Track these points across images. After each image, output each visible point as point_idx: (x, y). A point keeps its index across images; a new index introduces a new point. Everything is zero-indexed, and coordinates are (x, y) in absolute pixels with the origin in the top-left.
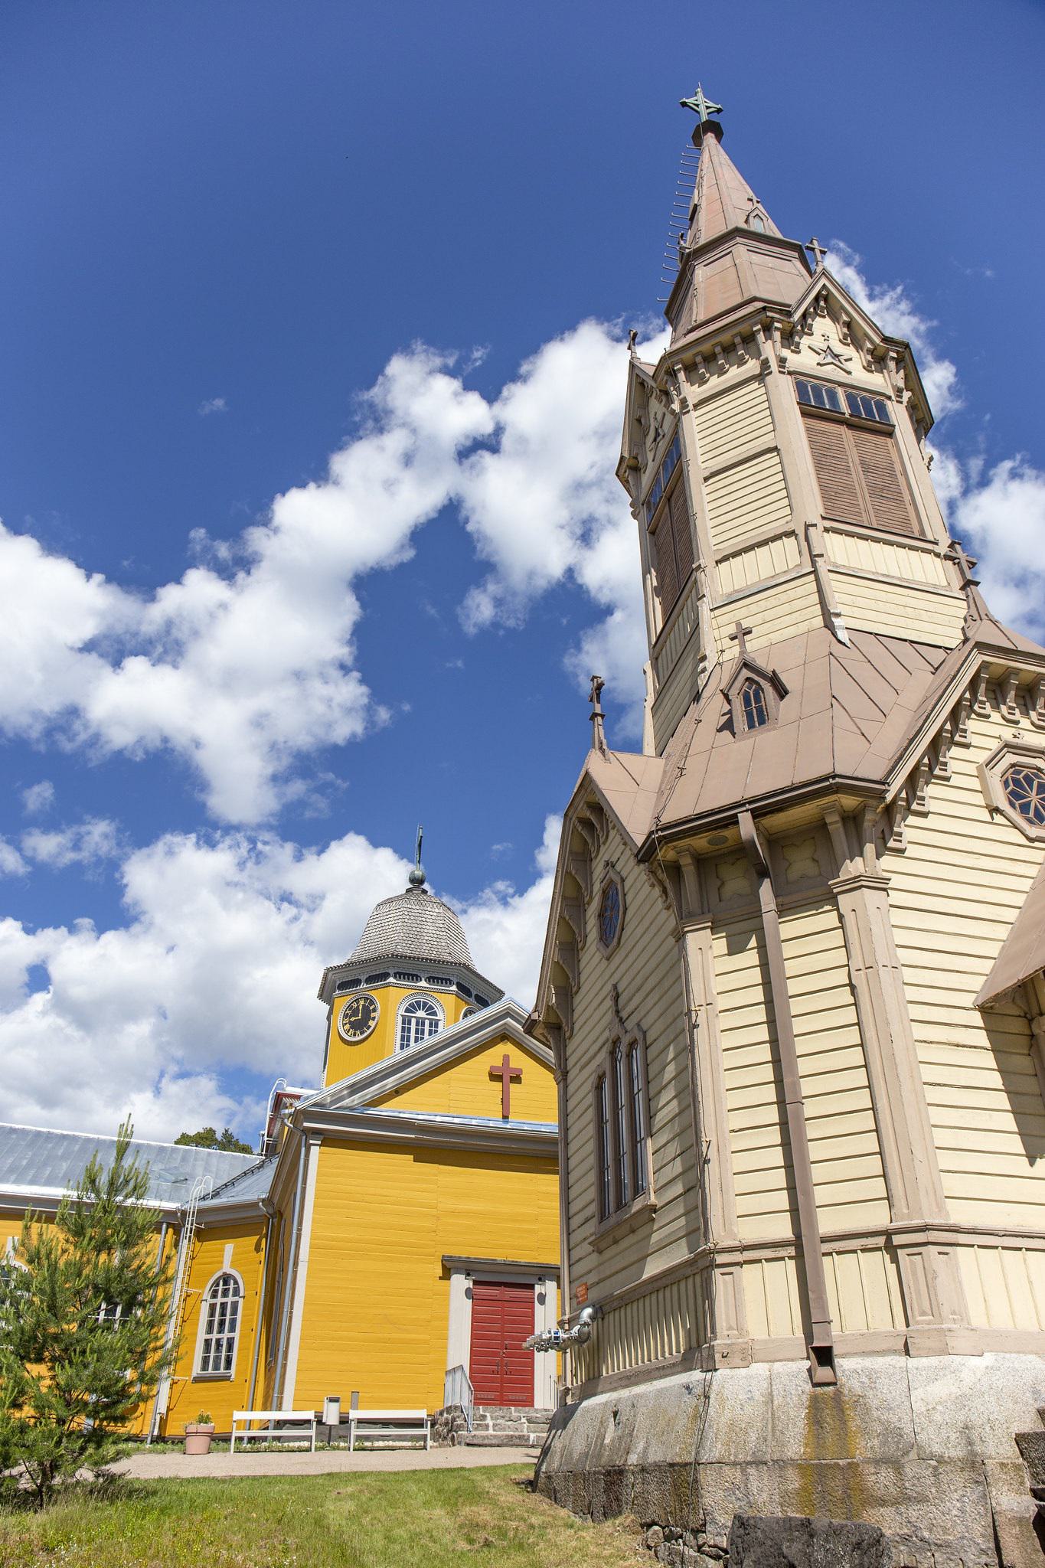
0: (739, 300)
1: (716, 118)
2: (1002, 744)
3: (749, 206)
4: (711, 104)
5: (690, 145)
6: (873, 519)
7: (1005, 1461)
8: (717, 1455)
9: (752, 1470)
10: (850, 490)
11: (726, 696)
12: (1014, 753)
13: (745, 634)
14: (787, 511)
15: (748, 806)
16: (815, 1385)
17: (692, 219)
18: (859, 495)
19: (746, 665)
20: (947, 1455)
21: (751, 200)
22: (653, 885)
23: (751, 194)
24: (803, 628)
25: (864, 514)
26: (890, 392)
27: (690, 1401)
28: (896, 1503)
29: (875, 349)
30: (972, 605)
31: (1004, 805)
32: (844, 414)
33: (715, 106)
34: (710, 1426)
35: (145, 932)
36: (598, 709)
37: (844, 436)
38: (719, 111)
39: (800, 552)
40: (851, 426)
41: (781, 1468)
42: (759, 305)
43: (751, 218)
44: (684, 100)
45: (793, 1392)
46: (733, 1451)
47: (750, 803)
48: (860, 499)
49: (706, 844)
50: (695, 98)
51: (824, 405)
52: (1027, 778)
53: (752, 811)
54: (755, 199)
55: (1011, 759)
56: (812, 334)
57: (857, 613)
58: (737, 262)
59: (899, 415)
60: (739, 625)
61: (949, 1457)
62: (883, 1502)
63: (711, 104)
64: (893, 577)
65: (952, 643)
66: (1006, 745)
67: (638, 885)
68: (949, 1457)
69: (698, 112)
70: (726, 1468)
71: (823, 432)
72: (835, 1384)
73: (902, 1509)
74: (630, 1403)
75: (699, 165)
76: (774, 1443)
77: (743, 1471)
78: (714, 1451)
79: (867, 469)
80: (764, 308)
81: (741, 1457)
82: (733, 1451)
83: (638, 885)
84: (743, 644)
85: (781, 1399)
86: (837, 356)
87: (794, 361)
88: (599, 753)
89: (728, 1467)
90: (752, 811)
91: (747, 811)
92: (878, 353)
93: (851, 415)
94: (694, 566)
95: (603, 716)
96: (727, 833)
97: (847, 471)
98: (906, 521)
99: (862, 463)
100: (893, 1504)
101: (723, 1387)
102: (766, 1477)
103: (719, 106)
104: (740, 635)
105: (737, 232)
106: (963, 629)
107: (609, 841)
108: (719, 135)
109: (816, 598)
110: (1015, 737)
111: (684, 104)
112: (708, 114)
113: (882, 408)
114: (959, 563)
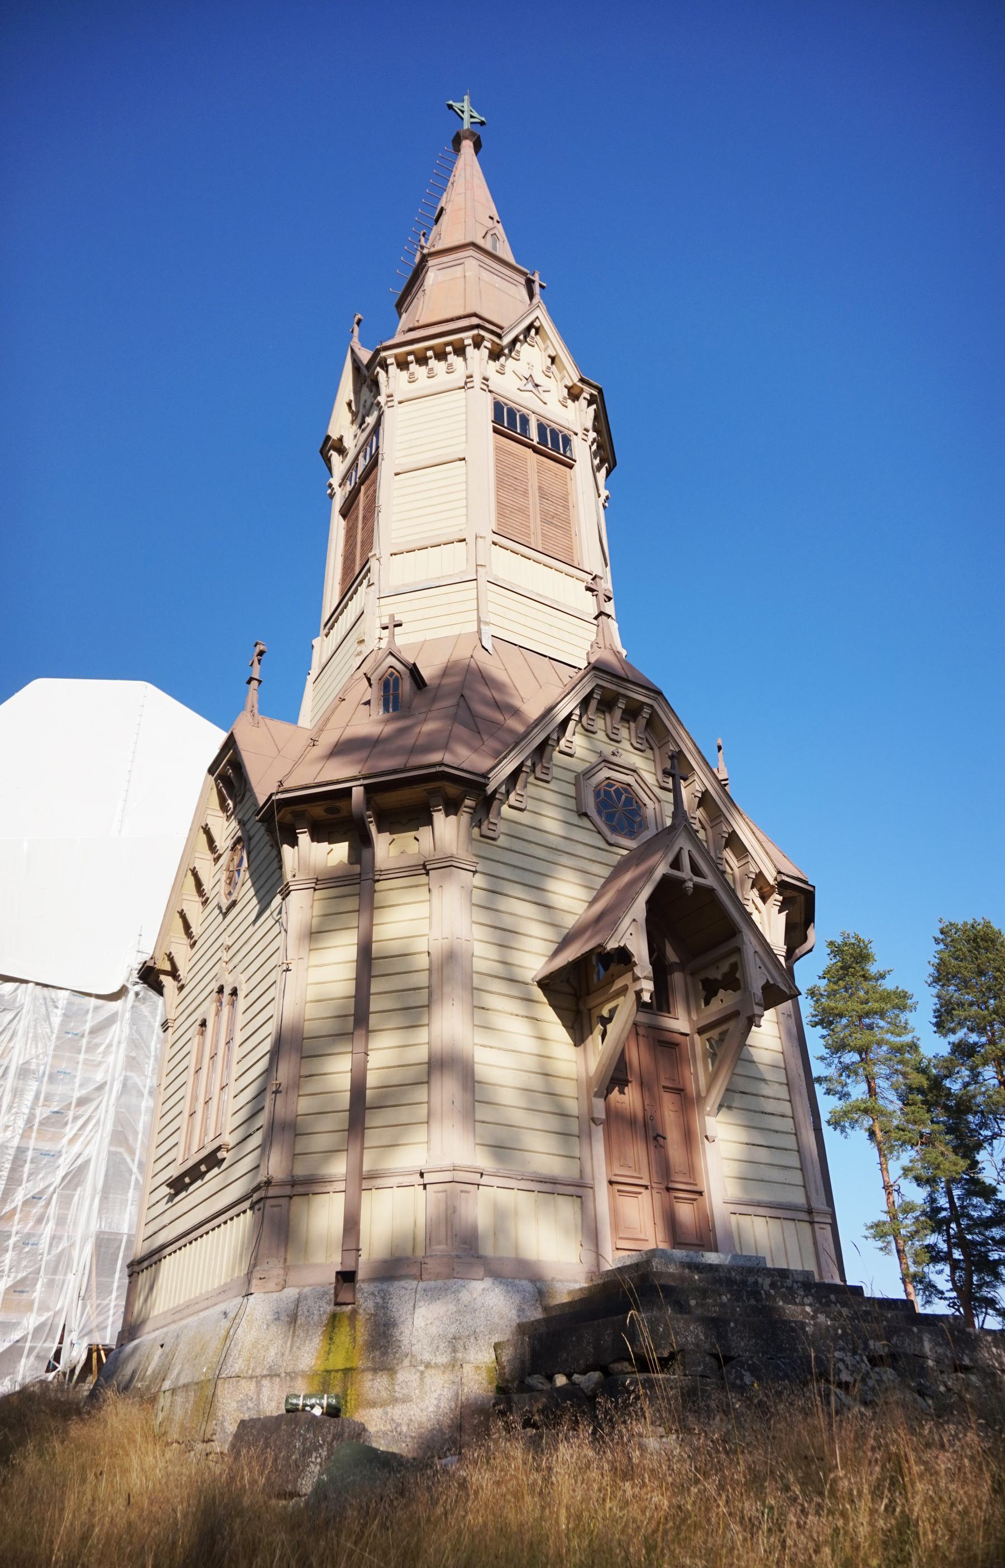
0: (460, 312)
1: (478, 130)
2: (601, 759)
3: (490, 223)
4: (475, 114)
5: (449, 147)
6: (540, 542)
7: (480, 1365)
8: (237, 1370)
9: (266, 1382)
10: (524, 511)
11: (369, 680)
12: (609, 768)
13: (396, 626)
14: (463, 519)
15: (361, 782)
16: (337, 1304)
17: (437, 221)
18: (531, 517)
19: (391, 653)
20: (433, 1362)
21: (491, 218)
22: (272, 846)
23: (494, 213)
24: (455, 631)
25: (532, 536)
26: (580, 431)
27: (225, 1324)
28: (383, 1404)
29: (572, 387)
30: (601, 634)
31: (591, 808)
32: (532, 440)
33: (479, 118)
34: (236, 1345)
35: (145, 962)
36: (256, 672)
37: (528, 461)
38: (482, 123)
39: (467, 560)
40: (536, 450)
41: (292, 1379)
42: (475, 321)
43: (488, 236)
44: (451, 102)
45: (315, 1312)
46: (252, 1366)
47: (364, 778)
48: (532, 521)
49: (323, 813)
50: (462, 104)
51: (516, 429)
52: (617, 791)
53: (365, 786)
54: (497, 217)
55: (605, 773)
56: (519, 360)
57: (506, 624)
58: (467, 274)
59: (582, 450)
60: (392, 616)
61: (435, 1363)
62: (373, 1404)
63: (475, 114)
64: (546, 597)
65: (583, 667)
66: (604, 761)
67: (262, 844)
68: (435, 1363)
69: (462, 119)
70: (243, 1382)
71: (511, 454)
72: (354, 1304)
73: (389, 1409)
74: (175, 1334)
75: (454, 170)
76: (290, 1358)
77: (258, 1383)
78: (237, 1365)
79: (543, 495)
80: (478, 326)
81: (258, 1372)
82: (252, 1366)
83: (262, 844)
84: (393, 635)
85: (303, 1319)
86: (537, 386)
87: (497, 382)
88: (249, 715)
89: (244, 1380)
90: (365, 786)
91: (361, 785)
92: (573, 391)
93: (538, 443)
94: (370, 555)
95: (260, 682)
96: (341, 804)
97: (525, 493)
98: (570, 549)
99: (540, 488)
100: (381, 1406)
101: (254, 1309)
102: (276, 1387)
103: (483, 119)
104: (391, 626)
105: (474, 245)
106: (588, 654)
107: (245, 800)
108: (477, 146)
109: (474, 604)
110: (614, 754)
111: (450, 107)
112: (472, 123)
113: (567, 441)
114: (596, 595)
